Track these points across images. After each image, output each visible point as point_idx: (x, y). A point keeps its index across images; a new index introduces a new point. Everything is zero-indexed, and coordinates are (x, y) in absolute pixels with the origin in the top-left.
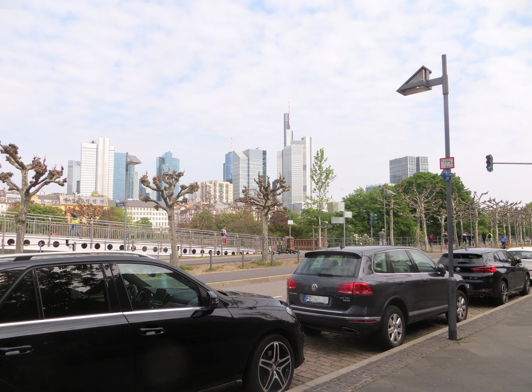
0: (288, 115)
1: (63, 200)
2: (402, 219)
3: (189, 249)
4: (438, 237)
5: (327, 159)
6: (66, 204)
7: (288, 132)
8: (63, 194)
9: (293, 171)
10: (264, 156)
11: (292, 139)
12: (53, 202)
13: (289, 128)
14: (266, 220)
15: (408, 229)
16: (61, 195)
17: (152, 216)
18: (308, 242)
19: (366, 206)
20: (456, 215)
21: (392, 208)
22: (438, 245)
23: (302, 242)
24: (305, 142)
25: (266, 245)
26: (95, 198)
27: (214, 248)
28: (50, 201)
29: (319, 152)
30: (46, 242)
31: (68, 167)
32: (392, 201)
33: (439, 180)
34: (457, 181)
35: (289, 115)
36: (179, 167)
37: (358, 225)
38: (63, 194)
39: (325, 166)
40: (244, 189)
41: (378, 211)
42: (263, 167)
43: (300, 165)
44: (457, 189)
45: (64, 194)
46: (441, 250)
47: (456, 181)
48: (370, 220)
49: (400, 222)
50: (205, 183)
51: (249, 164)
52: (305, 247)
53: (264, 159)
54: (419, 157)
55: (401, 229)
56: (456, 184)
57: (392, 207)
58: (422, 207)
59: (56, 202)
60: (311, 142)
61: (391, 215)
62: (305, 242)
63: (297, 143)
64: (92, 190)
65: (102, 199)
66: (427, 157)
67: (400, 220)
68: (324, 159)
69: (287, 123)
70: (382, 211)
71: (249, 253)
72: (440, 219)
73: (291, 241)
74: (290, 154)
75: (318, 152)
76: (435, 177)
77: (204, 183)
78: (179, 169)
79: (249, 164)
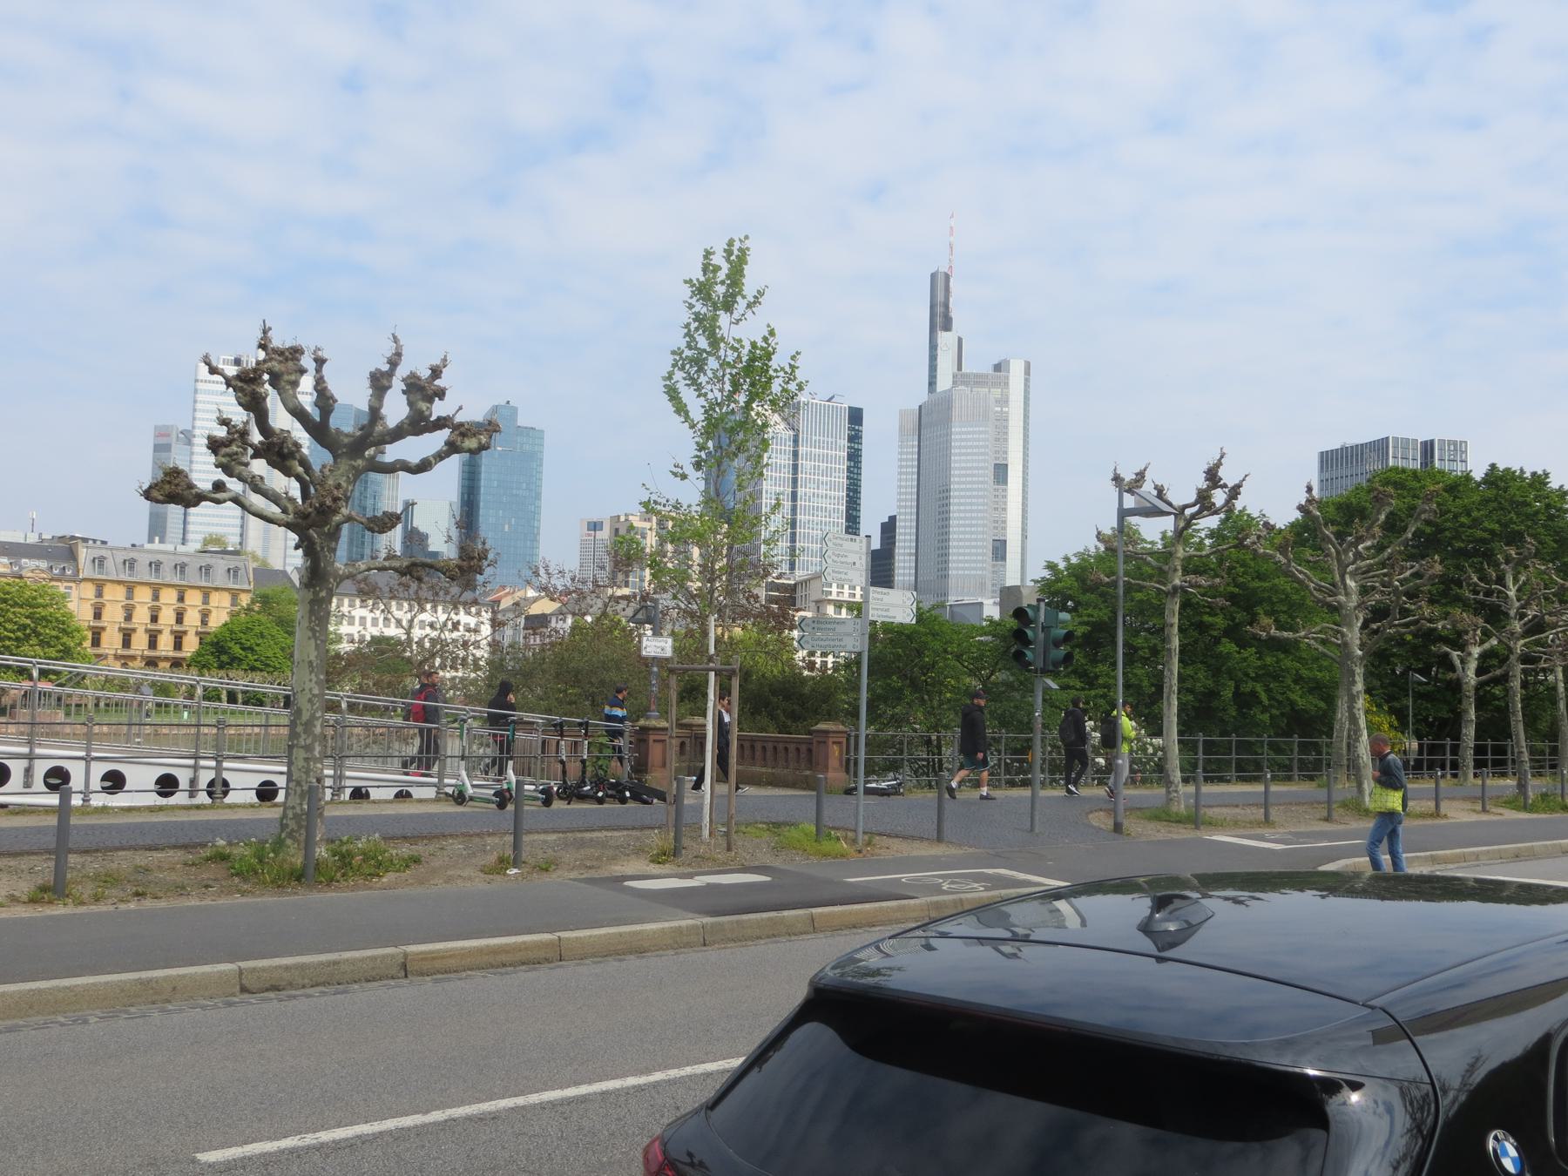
0: (947, 277)
1: (89, 562)
2: (1300, 659)
3: (24, 763)
4: (1448, 741)
5: (761, 293)
6: (130, 579)
7: (946, 340)
8: (91, 542)
9: (958, 483)
10: (854, 429)
11: (960, 368)
12: (51, 567)
13: (947, 326)
14: (312, 612)
15: (1322, 705)
16: (85, 544)
17: (192, 619)
18: (775, 748)
19: (1141, 601)
20: (1522, 642)
21: (1175, 588)
22: (1449, 776)
23: (753, 747)
24: (1007, 378)
25: (306, 760)
26: (207, 560)
27: (191, 762)
28: (44, 564)
29: (718, 259)
30: (184, 783)
31: (155, 451)
32: (1176, 551)
33: (1476, 498)
34: (1555, 507)
35: (951, 280)
36: (541, 460)
37: (1101, 681)
38: (91, 542)
39: (741, 330)
40: (221, 432)
41: (1192, 624)
42: (848, 468)
43: (985, 461)
44: (1555, 541)
45: (95, 541)
46: (1437, 806)
47: (1548, 506)
48: (1030, 643)
49: (1287, 670)
50: (626, 520)
51: (795, 454)
52: (764, 770)
53: (855, 438)
54: (1432, 442)
55: (1292, 703)
56: (1551, 518)
57: (1177, 582)
58: (1347, 594)
59: (64, 568)
60: (1027, 381)
61: (1172, 625)
62: (764, 748)
63: (978, 380)
64: (200, 532)
65: (232, 562)
66: (1466, 442)
67: (1288, 663)
68: (744, 297)
69: (939, 310)
70: (1212, 625)
71: (415, 796)
72: (1457, 662)
73: (652, 738)
74: (946, 421)
75: (708, 254)
76: (1461, 488)
77: (622, 519)
78: (541, 465)
79: (795, 454)
